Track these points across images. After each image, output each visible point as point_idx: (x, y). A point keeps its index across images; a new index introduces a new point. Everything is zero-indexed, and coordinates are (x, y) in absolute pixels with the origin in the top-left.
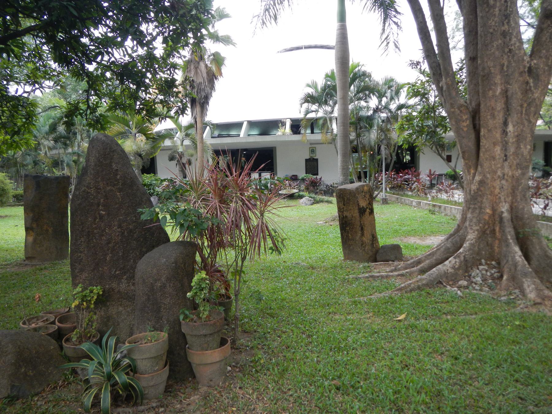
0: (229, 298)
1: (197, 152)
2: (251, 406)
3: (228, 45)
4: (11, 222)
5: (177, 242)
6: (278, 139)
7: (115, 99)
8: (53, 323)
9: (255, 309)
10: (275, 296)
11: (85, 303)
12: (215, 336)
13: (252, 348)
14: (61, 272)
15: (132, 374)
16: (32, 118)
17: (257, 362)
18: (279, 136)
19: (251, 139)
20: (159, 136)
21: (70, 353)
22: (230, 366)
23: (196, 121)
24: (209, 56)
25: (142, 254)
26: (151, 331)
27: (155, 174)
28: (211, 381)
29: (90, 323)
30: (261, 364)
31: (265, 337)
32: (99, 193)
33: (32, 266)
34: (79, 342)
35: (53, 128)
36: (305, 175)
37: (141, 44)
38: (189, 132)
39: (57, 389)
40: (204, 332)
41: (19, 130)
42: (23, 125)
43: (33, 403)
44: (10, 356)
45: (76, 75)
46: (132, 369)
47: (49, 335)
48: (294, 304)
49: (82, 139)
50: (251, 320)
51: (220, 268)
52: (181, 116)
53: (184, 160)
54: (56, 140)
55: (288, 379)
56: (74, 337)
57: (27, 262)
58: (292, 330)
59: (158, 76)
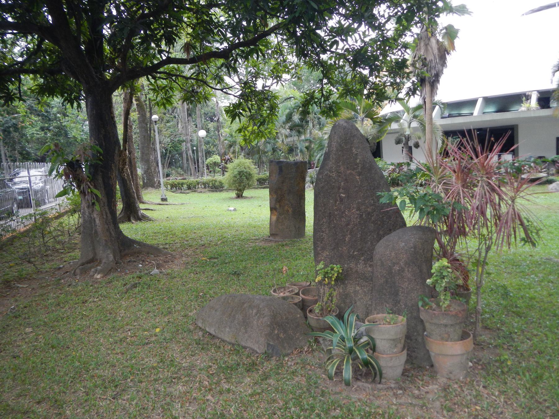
0: (468, 289)
1: (425, 134)
2: (498, 409)
3: (463, 15)
4: (256, 203)
5: (414, 227)
6: (522, 116)
7: (346, 85)
8: (298, 294)
9: (497, 305)
10: (522, 293)
11: (326, 279)
12: (457, 328)
13: (496, 347)
14: (300, 249)
15: (371, 352)
16: (275, 110)
17: (503, 362)
18: (522, 111)
19: (488, 118)
20: (385, 120)
21: (313, 323)
22: (471, 362)
23: (425, 102)
24: (441, 30)
25: (380, 238)
26: (389, 313)
27: (380, 157)
28: (451, 373)
29: (330, 298)
30: (507, 366)
31: (511, 337)
32: (340, 176)
33: (276, 242)
34: (321, 314)
35: (289, 117)
36: (556, 156)
37: (374, 28)
38: (417, 113)
39: (303, 353)
40: (445, 322)
41: (264, 121)
42: (268, 117)
43: (284, 362)
44: (266, 318)
45: (312, 66)
46: (372, 347)
47: (296, 304)
48: (546, 305)
49: (313, 126)
50: (493, 316)
51: (459, 258)
52: (412, 97)
53: (411, 143)
54: (291, 129)
55: (542, 388)
56: (317, 308)
57: (271, 238)
58: (545, 334)
59: (388, 58)
